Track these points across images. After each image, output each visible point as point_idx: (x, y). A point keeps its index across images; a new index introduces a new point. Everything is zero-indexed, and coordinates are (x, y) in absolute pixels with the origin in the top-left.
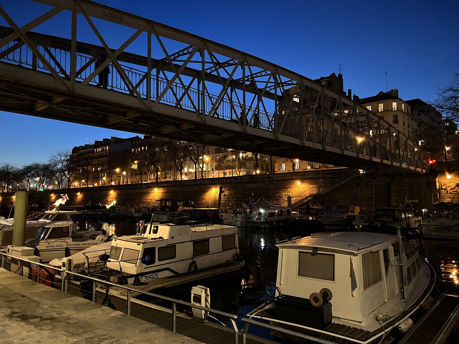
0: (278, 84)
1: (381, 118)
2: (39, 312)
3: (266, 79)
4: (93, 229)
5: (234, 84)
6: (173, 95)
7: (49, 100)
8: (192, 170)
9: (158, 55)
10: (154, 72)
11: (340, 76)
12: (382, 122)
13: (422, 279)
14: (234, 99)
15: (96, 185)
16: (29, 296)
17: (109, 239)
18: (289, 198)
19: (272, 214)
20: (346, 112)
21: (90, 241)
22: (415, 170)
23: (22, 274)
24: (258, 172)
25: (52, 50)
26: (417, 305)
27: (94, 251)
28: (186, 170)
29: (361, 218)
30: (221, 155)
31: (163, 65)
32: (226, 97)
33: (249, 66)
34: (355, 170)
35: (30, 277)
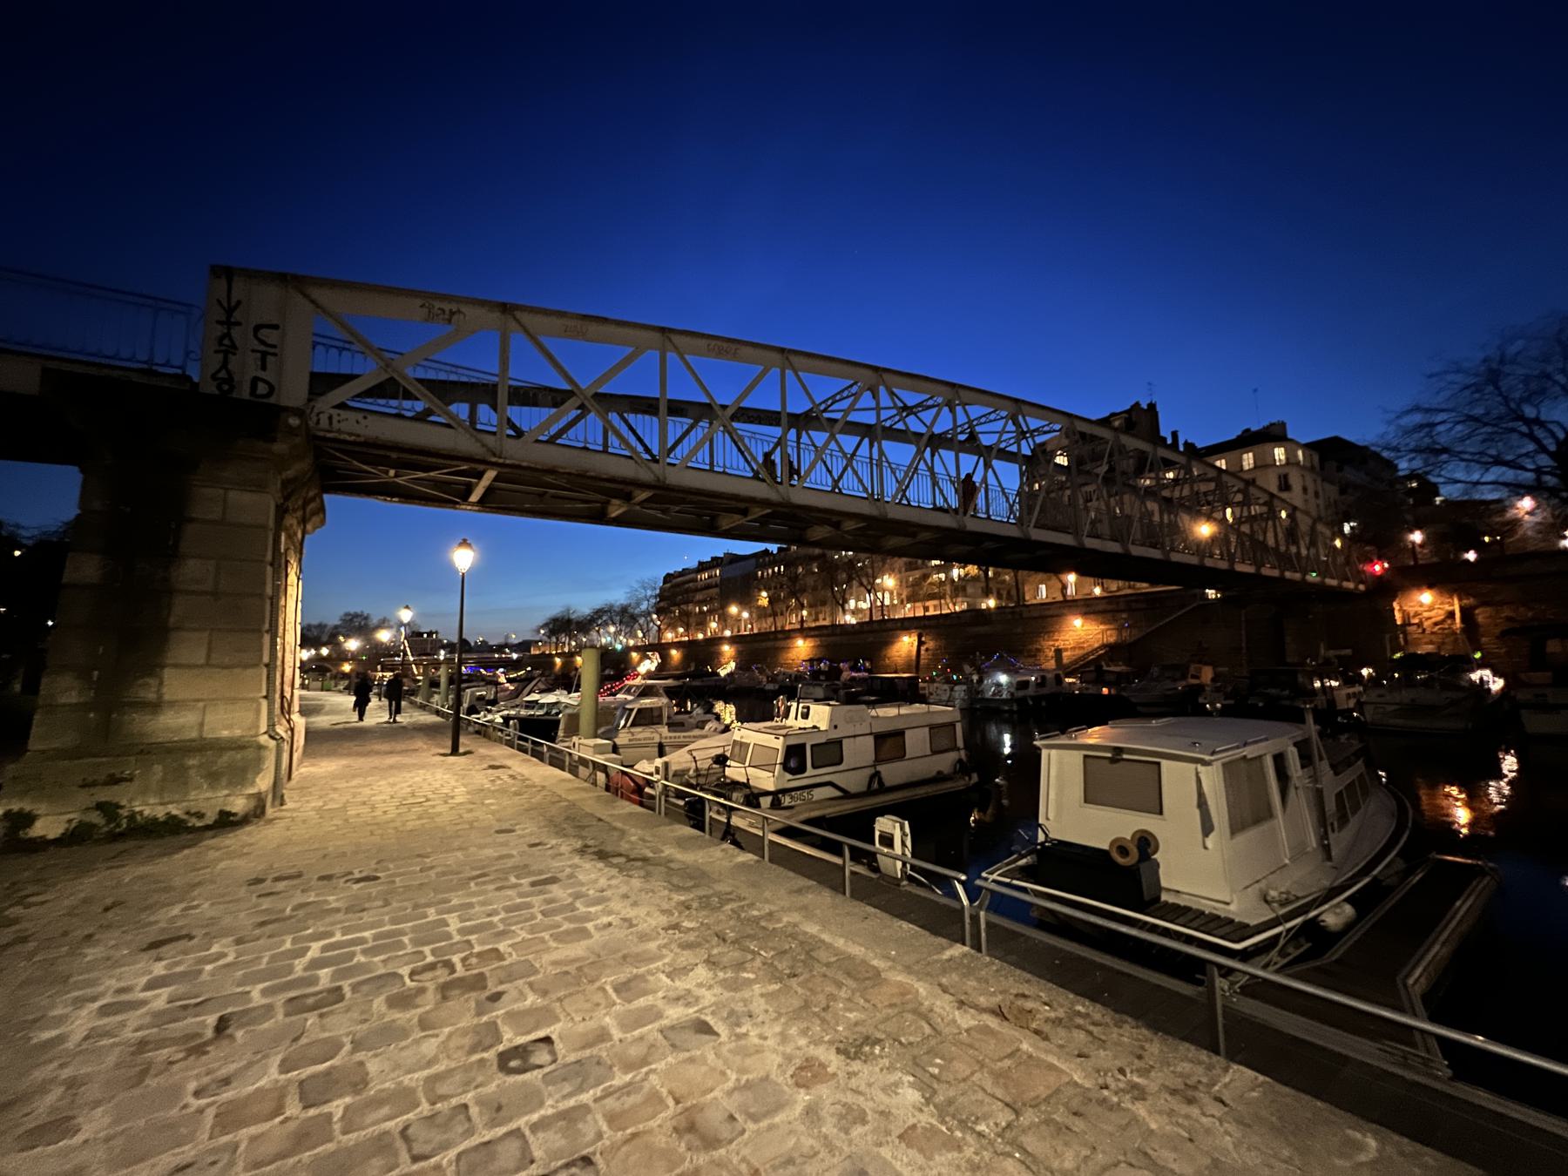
0: (1024, 433)
1: (1251, 483)
2: (624, 847)
3: (999, 426)
4: (699, 711)
5: (937, 442)
6: (833, 473)
7: (627, 497)
8: (864, 605)
9: (798, 406)
10: (792, 433)
11: (1152, 406)
12: (1252, 490)
13: (1374, 822)
14: (938, 468)
15: (700, 636)
16: (608, 819)
17: (727, 729)
18: (1059, 652)
19: (1023, 685)
20: (1171, 475)
21: (696, 732)
22: (1304, 579)
23: (595, 783)
24: (992, 603)
25: (631, 417)
26: (1366, 875)
27: (705, 747)
28: (852, 604)
29: (1217, 690)
30: (918, 574)
31: (804, 422)
32: (922, 466)
33: (964, 405)
34: (1197, 591)
35: (608, 788)
